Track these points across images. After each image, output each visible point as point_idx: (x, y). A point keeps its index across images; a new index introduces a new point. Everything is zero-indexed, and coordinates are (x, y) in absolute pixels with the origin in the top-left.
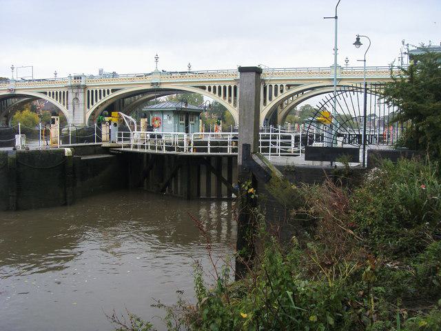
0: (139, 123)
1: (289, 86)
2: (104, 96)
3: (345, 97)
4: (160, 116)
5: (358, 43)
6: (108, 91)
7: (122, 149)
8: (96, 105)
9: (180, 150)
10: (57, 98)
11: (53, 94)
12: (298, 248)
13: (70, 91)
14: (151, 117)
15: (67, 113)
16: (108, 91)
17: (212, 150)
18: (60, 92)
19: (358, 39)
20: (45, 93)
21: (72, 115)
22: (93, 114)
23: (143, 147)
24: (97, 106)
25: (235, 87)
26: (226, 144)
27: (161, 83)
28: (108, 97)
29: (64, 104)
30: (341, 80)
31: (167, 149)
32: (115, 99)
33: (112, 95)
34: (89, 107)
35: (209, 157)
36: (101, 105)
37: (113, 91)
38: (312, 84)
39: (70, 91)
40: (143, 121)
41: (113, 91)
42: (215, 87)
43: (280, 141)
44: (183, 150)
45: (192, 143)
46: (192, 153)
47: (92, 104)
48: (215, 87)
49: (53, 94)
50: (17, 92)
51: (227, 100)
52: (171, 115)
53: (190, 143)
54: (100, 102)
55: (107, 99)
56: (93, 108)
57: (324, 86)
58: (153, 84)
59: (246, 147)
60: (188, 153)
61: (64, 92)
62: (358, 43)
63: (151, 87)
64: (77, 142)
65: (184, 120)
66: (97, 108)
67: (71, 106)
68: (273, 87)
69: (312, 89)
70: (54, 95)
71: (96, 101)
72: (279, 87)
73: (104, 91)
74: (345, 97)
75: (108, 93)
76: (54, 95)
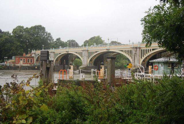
4: (158, 65)
6: (151, 50)
8: (145, 57)
10: (126, 52)
11: (127, 51)
12: (110, 120)
14: (154, 65)
16: (151, 50)
18: (147, 50)
20: (122, 51)
21: (134, 61)
22: (144, 61)
24: (145, 57)
27: (109, 49)
28: (150, 53)
29: (129, 55)
32: (154, 54)
34: (141, 58)
36: (148, 56)
37: (96, 52)
39: (133, 50)
41: (96, 52)
45: (154, 79)
47: (143, 56)
49: (127, 51)
50: (110, 50)
51: (128, 55)
52: (163, 64)
53: (153, 79)
54: (147, 55)
56: (143, 58)
61: (130, 50)
65: (171, 66)
66: (146, 58)
67: (133, 57)
68: (142, 50)
70: (125, 51)
71: (145, 55)
72: (150, 50)
73: (149, 50)
75: (150, 51)
76: (125, 51)
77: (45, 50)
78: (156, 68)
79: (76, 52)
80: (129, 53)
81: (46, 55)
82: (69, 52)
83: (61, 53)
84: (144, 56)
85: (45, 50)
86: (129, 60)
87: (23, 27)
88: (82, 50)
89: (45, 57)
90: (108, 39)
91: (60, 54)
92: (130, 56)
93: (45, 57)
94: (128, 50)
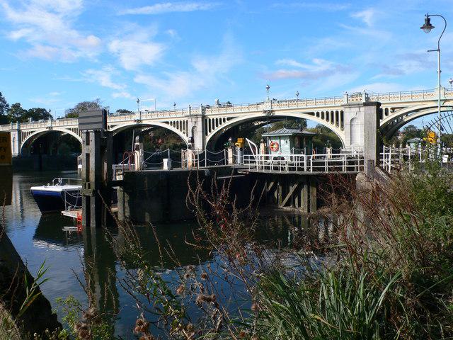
0: (259, 147)
1: (393, 109)
2: (221, 124)
3: (449, 120)
4: (278, 141)
5: (428, 25)
7: (249, 170)
9: (299, 169)
13: (189, 120)
15: (342, 135)
16: (224, 119)
17: (330, 169)
19: (428, 20)
23: (276, 168)
25: (342, 112)
26: (341, 163)
28: (224, 125)
30: (446, 101)
31: (290, 169)
33: (228, 123)
35: (326, 176)
37: (228, 119)
38: (416, 106)
39: (189, 120)
40: (262, 146)
41: (228, 119)
42: (323, 113)
43: (325, 166)
44: (303, 170)
46: (311, 171)
48: (323, 113)
55: (217, 131)
57: (429, 108)
58: (265, 112)
59: (371, 162)
60: (308, 173)
62: (428, 25)
63: (265, 115)
64: (318, 153)
69: (417, 111)
70: (174, 124)
74: (449, 120)
76: (174, 124)
77: (51, 151)
78: (275, 146)
79: (69, 127)
80: (337, 120)
81: (100, 119)
82: (54, 129)
83: (115, 124)
84: (212, 130)
85: (51, 151)
86: (179, 138)
87: (8, 231)
88: (342, 106)
89: (99, 116)
90: (138, 101)
91: (32, 132)
92: (332, 121)
93: (99, 116)
94: (335, 112)
